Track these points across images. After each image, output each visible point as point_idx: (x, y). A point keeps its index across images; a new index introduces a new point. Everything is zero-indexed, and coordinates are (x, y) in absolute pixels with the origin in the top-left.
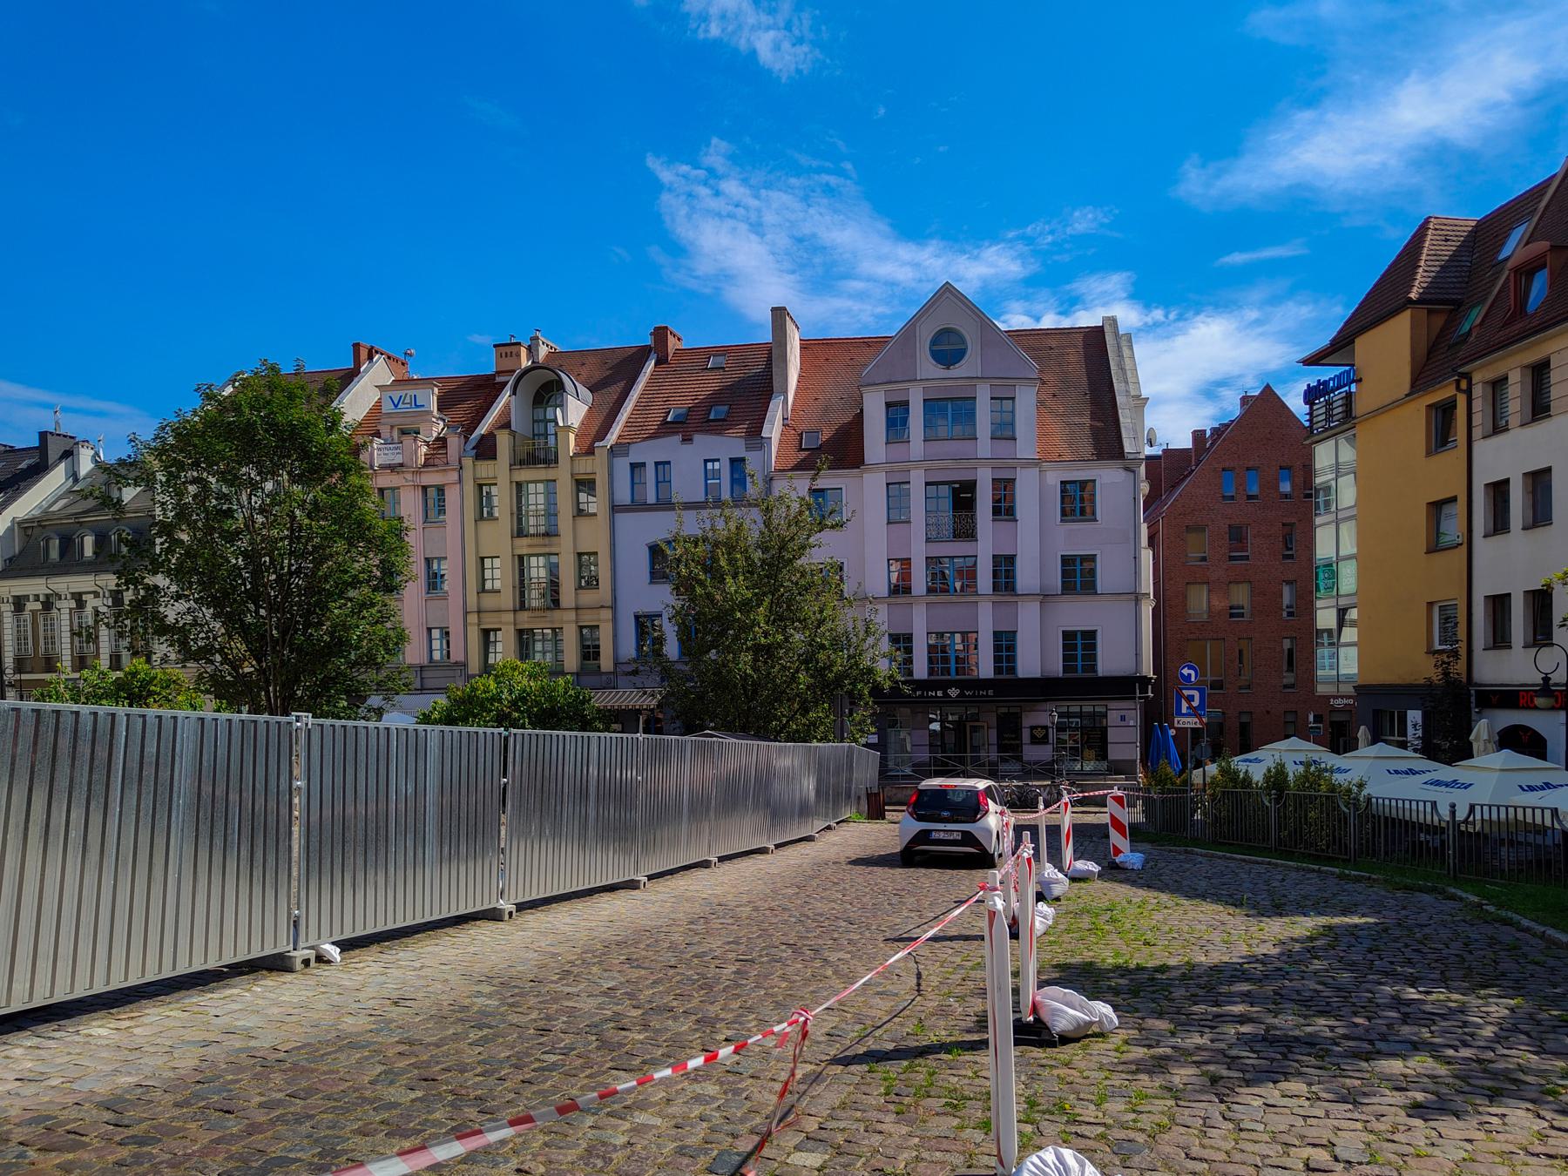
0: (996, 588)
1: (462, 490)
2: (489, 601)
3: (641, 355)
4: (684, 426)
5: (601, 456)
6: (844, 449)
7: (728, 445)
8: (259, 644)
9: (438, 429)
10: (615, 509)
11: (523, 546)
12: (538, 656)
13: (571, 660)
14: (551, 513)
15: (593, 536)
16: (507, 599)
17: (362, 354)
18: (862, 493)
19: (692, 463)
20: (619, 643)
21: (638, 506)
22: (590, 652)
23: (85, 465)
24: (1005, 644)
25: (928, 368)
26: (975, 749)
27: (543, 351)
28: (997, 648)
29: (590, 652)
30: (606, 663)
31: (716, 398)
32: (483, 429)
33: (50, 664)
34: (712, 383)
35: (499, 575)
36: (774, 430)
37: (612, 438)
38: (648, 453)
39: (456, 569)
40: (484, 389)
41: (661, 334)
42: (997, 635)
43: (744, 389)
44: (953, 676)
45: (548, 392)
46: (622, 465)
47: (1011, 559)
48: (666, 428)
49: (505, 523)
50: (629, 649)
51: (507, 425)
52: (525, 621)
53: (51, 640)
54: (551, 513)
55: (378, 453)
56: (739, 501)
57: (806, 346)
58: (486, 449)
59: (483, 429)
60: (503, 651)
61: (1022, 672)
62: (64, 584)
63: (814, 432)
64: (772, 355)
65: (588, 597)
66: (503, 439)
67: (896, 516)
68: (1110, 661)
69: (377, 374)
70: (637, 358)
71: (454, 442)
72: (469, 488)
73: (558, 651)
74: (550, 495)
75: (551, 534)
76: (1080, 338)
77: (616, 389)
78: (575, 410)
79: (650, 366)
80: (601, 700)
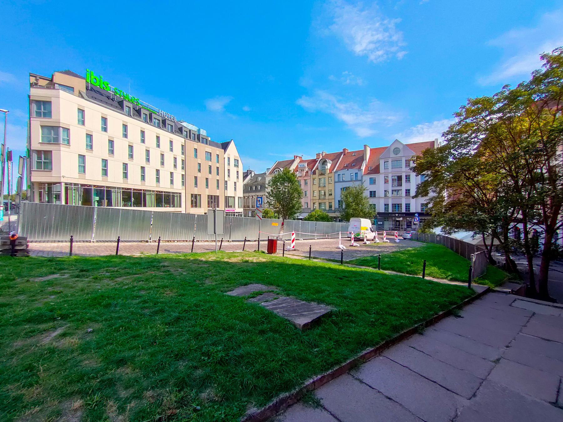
0: (406, 195)
1: (337, 261)
2: (314, 198)
3: (342, 153)
4: (348, 167)
5: (333, 174)
6: (376, 170)
7: (353, 171)
8: (283, 206)
9: (307, 169)
10: (335, 182)
11: (320, 189)
12: (510, 151)
13: (327, 208)
14: (324, 183)
15: (331, 187)
16: (317, 198)
17: (296, 157)
18: (380, 179)
19: (348, 174)
20: (335, 205)
21: (339, 182)
22: (330, 207)
23: (253, 175)
24: (408, 206)
25: (392, 155)
26: (402, 226)
27: (324, 154)
28: (406, 207)
29: (330, 207)
30: (333, 208)
31: (353, 161)
32: (314, 169)
33: (248, 207)
34: (353, 158)
35: (316, 194)
36: (363, 168)
37: (335, 170)
38: (340, 172)
39: (310, 196)
40: (315, 161)
41: (344, 150)
42: (406, 204)
43: (359, 159)
44: (397, 212)
45: (324, 162)
46: (337, 175)
47: (409, 190)
48: (345, 168)
49: (317, 186)
50: (337, 206)
51: (318, 169)
52: (320, 201)
53: (249, 203)
54: (324, 183)
55: (298, 174)
56: (357, 180)
57: (371, 150)
58: (314, 173)
59: (314, 169)
60: (317, 205)
61: (411, 211)
62: (251, 194)
63: (371, 167)
64: (363, 153)
65: (330, 197)
66: (317, 171)
67: (386, 181)
68: (412, 210)
69: (297, 161)
70: (339, 155)
71: (309, 172)
72: (312, 179)
73: (325, 207)
74: (324, 180)
75: (324, 186)
76: (429, 144)
77: (337, 160)
78: (329, 165)
79: (342, 156)
80: (331, 215)
